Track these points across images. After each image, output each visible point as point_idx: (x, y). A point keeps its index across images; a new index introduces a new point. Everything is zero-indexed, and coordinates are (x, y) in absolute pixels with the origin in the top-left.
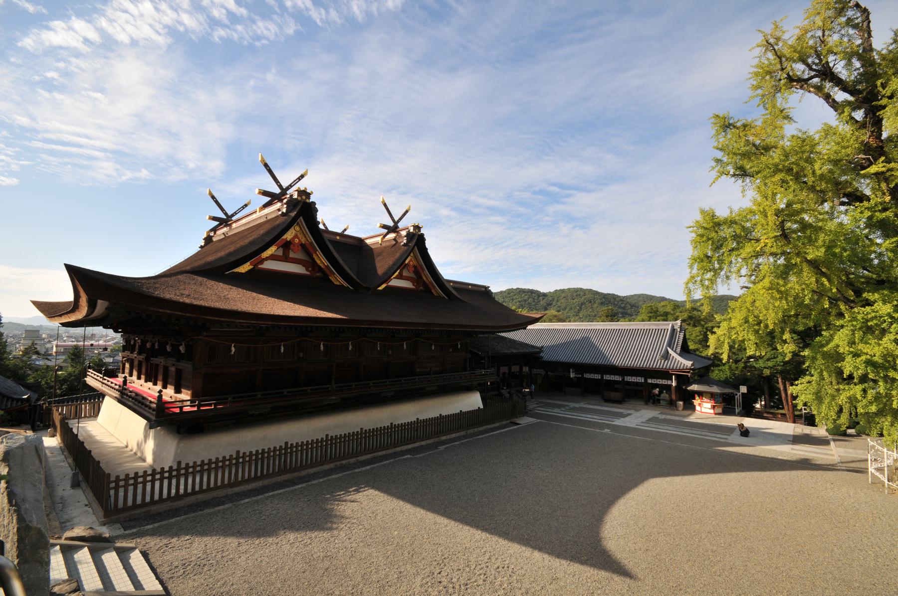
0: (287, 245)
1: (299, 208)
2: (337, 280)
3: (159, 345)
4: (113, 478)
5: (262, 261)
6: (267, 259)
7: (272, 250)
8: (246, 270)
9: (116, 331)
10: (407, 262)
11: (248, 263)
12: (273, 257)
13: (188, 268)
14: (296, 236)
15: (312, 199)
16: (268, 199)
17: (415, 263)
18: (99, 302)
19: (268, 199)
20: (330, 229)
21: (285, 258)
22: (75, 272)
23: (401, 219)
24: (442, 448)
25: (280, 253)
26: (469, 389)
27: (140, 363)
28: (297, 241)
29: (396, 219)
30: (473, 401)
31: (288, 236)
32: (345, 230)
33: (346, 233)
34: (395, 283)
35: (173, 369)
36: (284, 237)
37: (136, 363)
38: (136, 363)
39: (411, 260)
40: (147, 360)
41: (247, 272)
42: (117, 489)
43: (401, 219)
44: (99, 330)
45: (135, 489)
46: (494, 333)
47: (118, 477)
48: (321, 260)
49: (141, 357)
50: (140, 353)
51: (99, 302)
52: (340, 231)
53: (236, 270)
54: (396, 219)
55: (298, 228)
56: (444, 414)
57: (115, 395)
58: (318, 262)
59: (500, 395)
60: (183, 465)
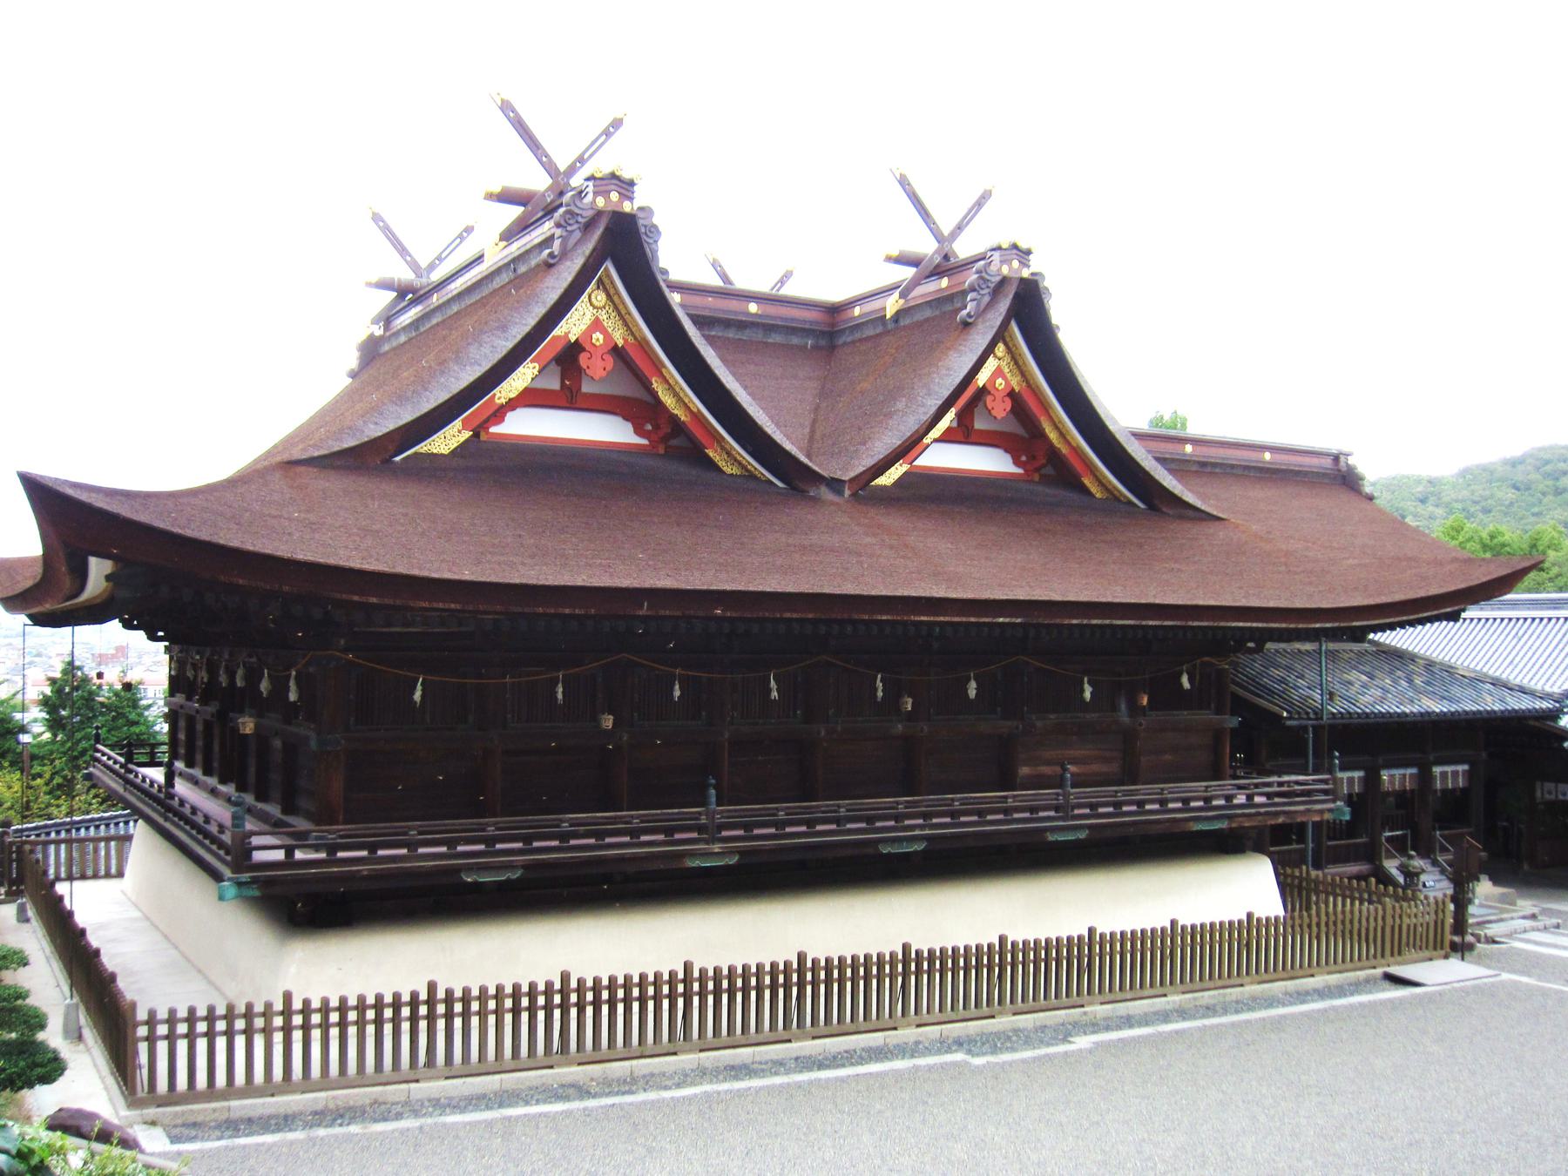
0: (570, 358)
1: (598, 233)
2: (730, 455)
3: (246, 678)
4: (142, 1015)
5: (499, 414)
6: (512, 404)
7: (523, 377)
8: (454, 444)
9: (153, 637)
10: (982, 378)
11: (458, 423)
12: (531, 398)
13: (297, 453)
14: (597, 325)
15: (641, 198)
16: (516, 211)
17: (1015, 382)
18: (93, 562)
19: (516, 211)
20: (741, 283)
21: (569, 398)
22: (42, 494)
23: (960, 227)
24: (1083, 1042)
25: (554, 384)
26: (1224, 843)
27: (208, 725)
28: (598, 338)
29: (946, 230)
30: (1245, 889)
31: (573, 326)
32: (782, 282)
33: (788, 291)
34: (942, 457)
35: (277, 743)
36: (558, 331)
37: (200, 727)
38: (200, 727)
39: (998, 372)
40: (222, 715)
41: (454, 452)
42: (151, 1039)
43: (960, 227)
44: (112, 632)
45: (717, 1003)
46: (1359, 635)
47: (152, 1013)
48: (676, 395)
49: (211, 709)
50: (204, 701)
51: (93, 562)
52: (763, 286)
53: (423, 448)
54: (946, 230)
55: (600, 298)
56: (1186, 920)
57: (857, 311)
58: (668, 400)
59: (1385, 879)
60: (297, 1005)
